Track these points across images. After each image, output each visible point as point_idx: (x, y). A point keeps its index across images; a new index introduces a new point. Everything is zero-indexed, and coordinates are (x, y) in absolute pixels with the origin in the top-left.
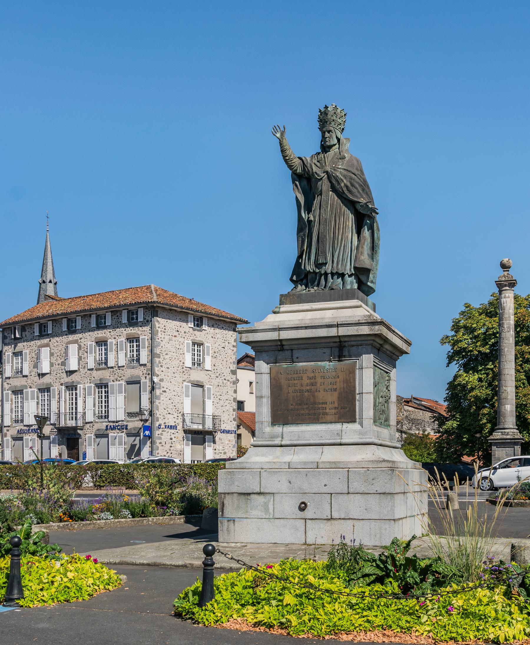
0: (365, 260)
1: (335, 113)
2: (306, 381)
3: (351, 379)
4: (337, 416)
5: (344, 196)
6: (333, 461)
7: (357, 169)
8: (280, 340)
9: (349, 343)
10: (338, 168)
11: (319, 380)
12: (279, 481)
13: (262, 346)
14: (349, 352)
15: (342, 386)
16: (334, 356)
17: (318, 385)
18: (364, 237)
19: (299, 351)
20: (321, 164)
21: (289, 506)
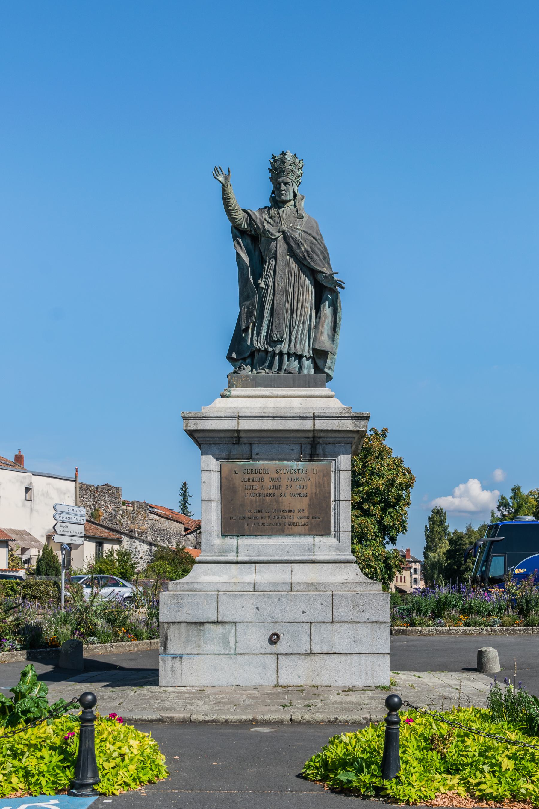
0: (324, 341)
1: (294, 162)
2: (267, 483)
3: (326, 483)
4: (307, 527)
5: (305, 263)
6: (311, 582)
7: (317, 233)
8: (238, 431)
9: (325, 439)
10: (297, 229)
11: (285, 483)
12: (243, 607)
14: (323, 450)
15: (314, 491)
16: (305, 454)
17: (284, 488)
18: (325, 314)
19: (260, 445)
20: (274, 221)
21: (255, 638)
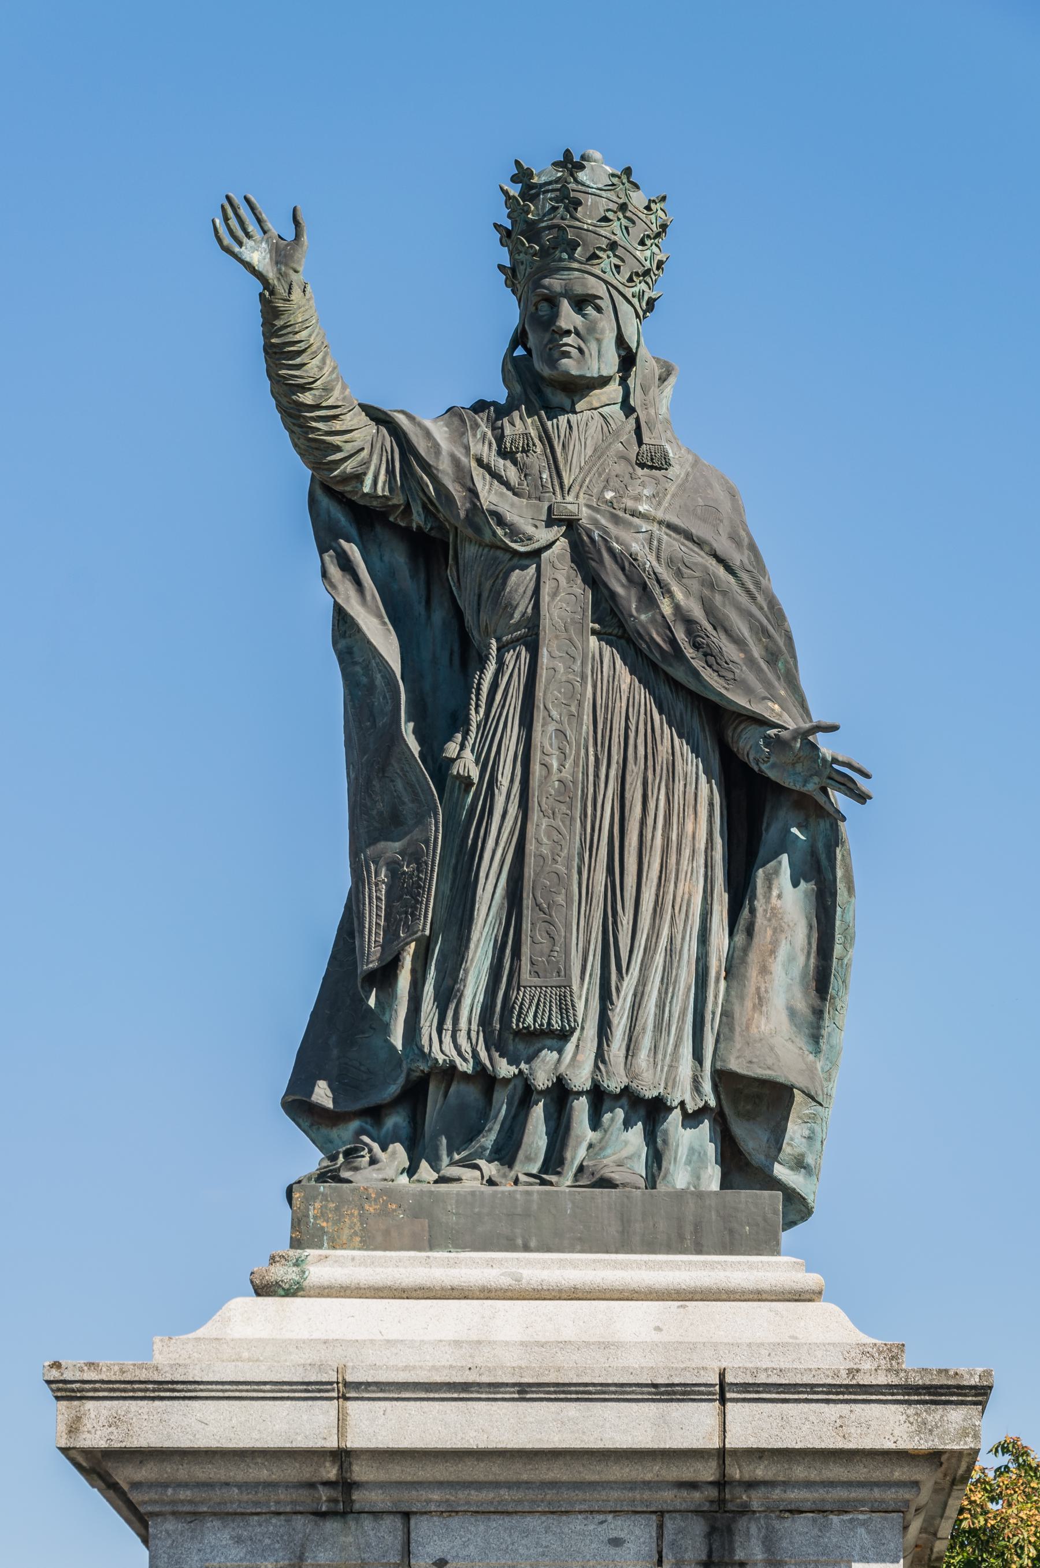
0: (770, 1038)
1: (623, 207)
5: (679, 674)
8: (342, 1456)
9: (777, 1494)
13: (209, 1485)
18: (774, 914)
19: (455, 1522)
20: (523, 470)
